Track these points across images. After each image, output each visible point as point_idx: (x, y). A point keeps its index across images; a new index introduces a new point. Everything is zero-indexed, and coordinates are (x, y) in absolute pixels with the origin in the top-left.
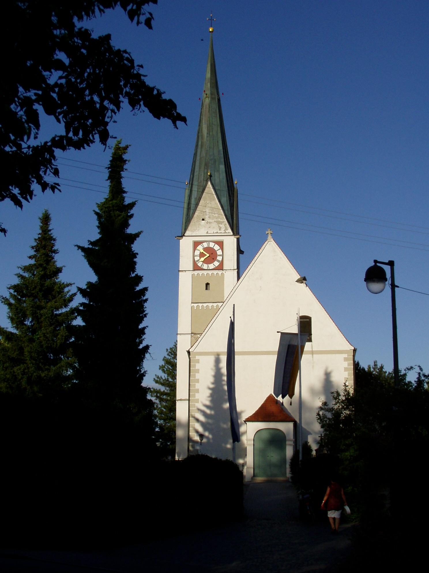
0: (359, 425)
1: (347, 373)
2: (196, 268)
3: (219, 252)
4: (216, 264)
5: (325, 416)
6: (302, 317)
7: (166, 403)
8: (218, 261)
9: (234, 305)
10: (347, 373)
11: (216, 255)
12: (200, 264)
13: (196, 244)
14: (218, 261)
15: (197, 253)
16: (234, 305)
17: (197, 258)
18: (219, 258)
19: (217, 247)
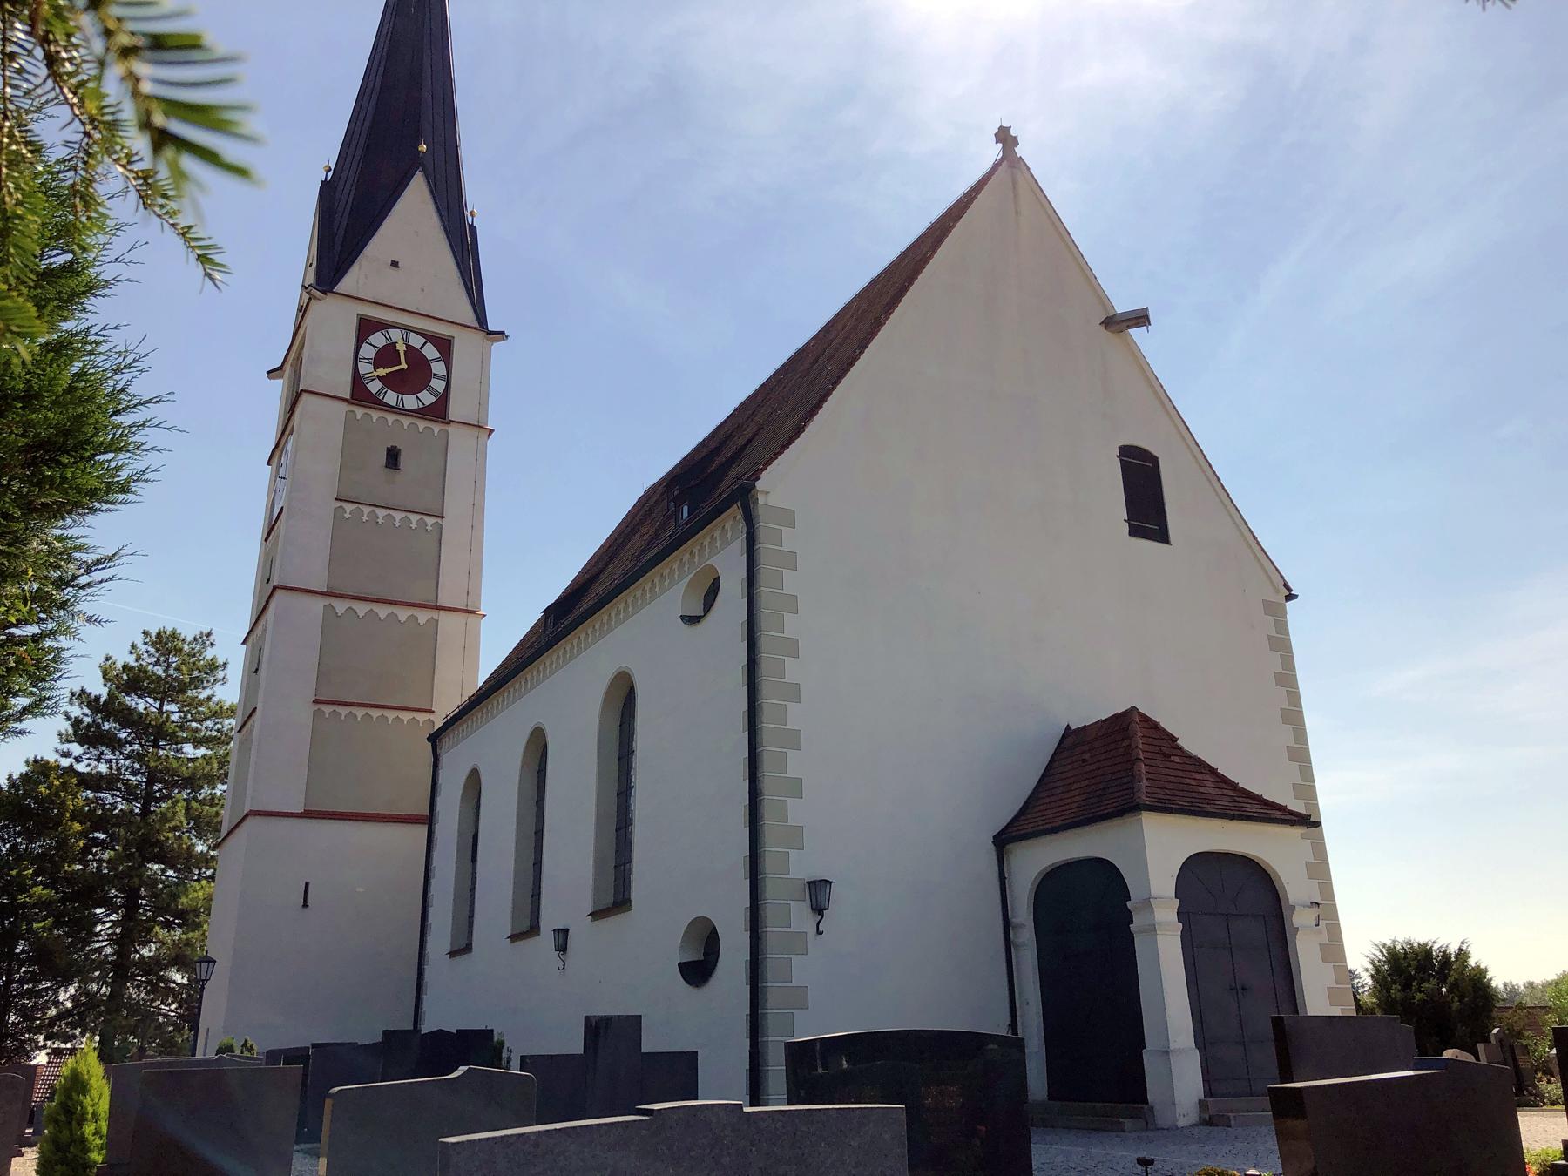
0: (23, 951)
1: (788, 589)
2: (360, 394)
3: (438, 368)
4: (427, 398)
5: (114, 933)
6: (1001, 128)
7: (51, 1018)
8: (433, 392)
9: (307, 885)
10: (788, 589)
11: (429, 375)
12: (374, 387)
13: (366, 327)
14: (433, 392)
15: (368, 352)
16: (307, 885)
17: (365, 368)
18: (438, 385)
19: (430, 352)
